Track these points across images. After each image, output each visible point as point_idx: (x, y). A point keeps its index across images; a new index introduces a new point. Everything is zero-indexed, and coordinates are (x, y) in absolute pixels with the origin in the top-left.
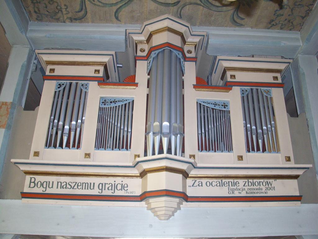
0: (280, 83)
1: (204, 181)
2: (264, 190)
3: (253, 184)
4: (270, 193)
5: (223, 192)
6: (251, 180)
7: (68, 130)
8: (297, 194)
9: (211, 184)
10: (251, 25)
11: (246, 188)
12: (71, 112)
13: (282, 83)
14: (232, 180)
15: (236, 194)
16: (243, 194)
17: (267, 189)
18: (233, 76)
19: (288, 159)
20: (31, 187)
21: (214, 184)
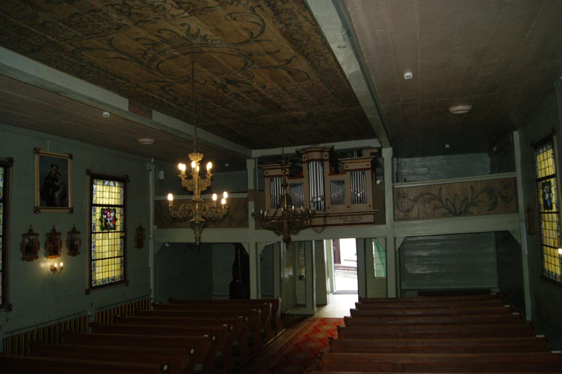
0: (255, 148)
1: (334, 218)
2: (358, 219)
3: (354, 218)
4: (361, 221)
5: (342, 222)
6: (353, 216)
7: (314, 224)
8: (373, 221)
9: (336, 219)
10: (195, 142)
11: (351, 220)
12: (338, 227)
13: (330, 161)
14: (345, 217)
15: (347, 222)
16: (350, 222)
17: (360, 219)
18: (347, 167)
19: (370, 206)
20: (306, 302)
21: (338, 218)
